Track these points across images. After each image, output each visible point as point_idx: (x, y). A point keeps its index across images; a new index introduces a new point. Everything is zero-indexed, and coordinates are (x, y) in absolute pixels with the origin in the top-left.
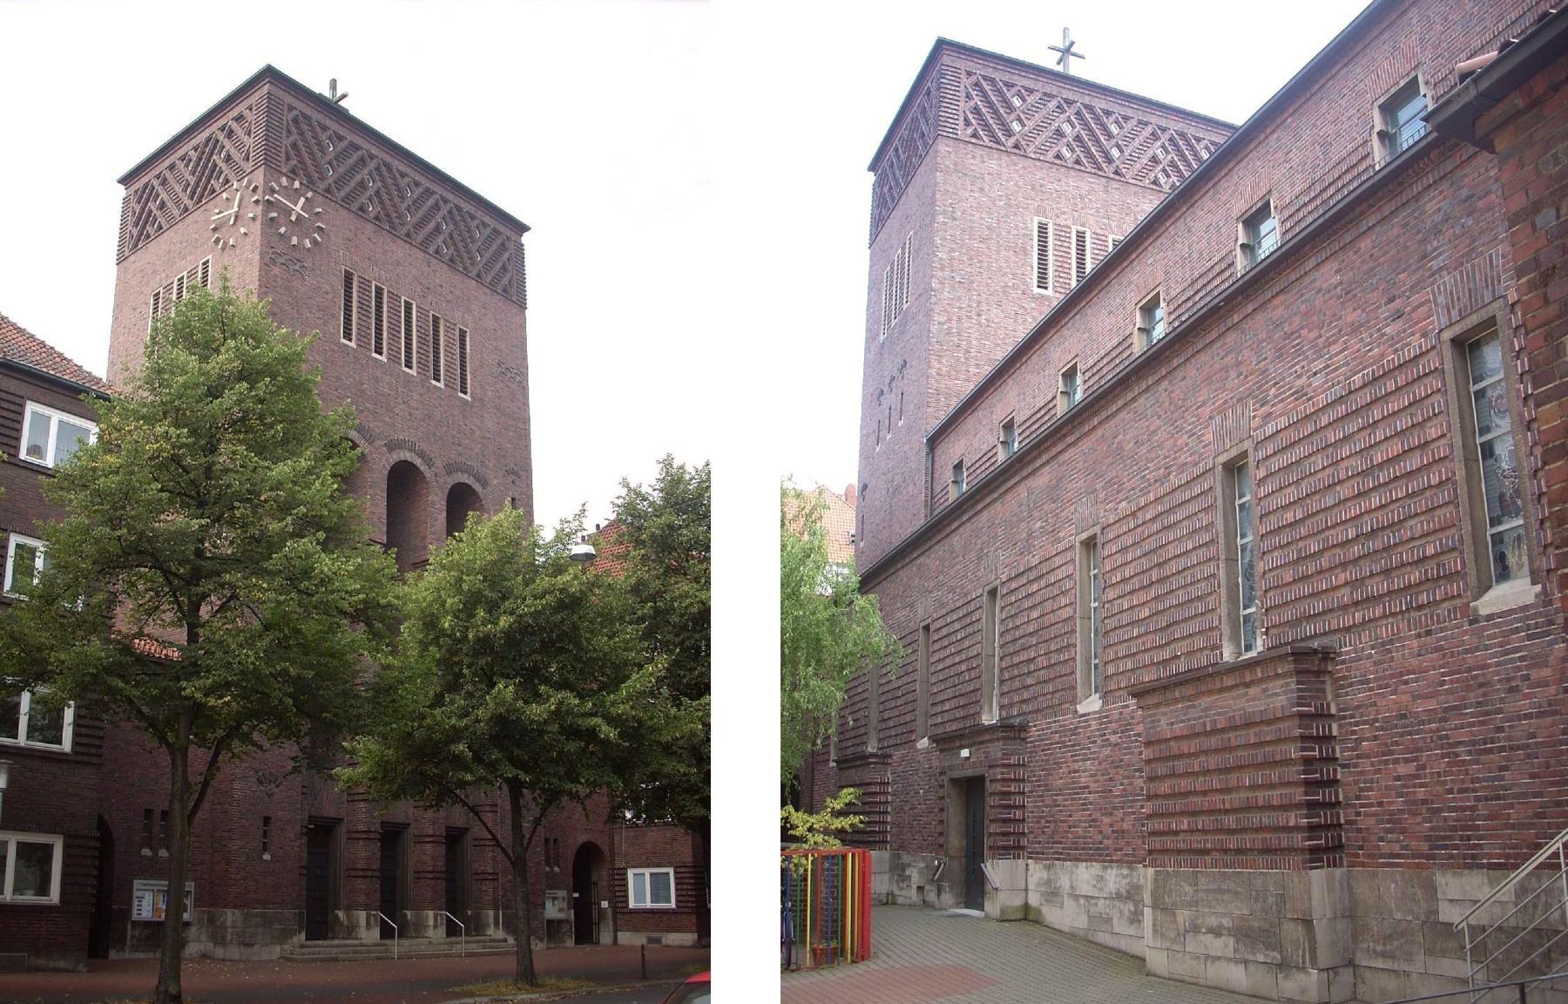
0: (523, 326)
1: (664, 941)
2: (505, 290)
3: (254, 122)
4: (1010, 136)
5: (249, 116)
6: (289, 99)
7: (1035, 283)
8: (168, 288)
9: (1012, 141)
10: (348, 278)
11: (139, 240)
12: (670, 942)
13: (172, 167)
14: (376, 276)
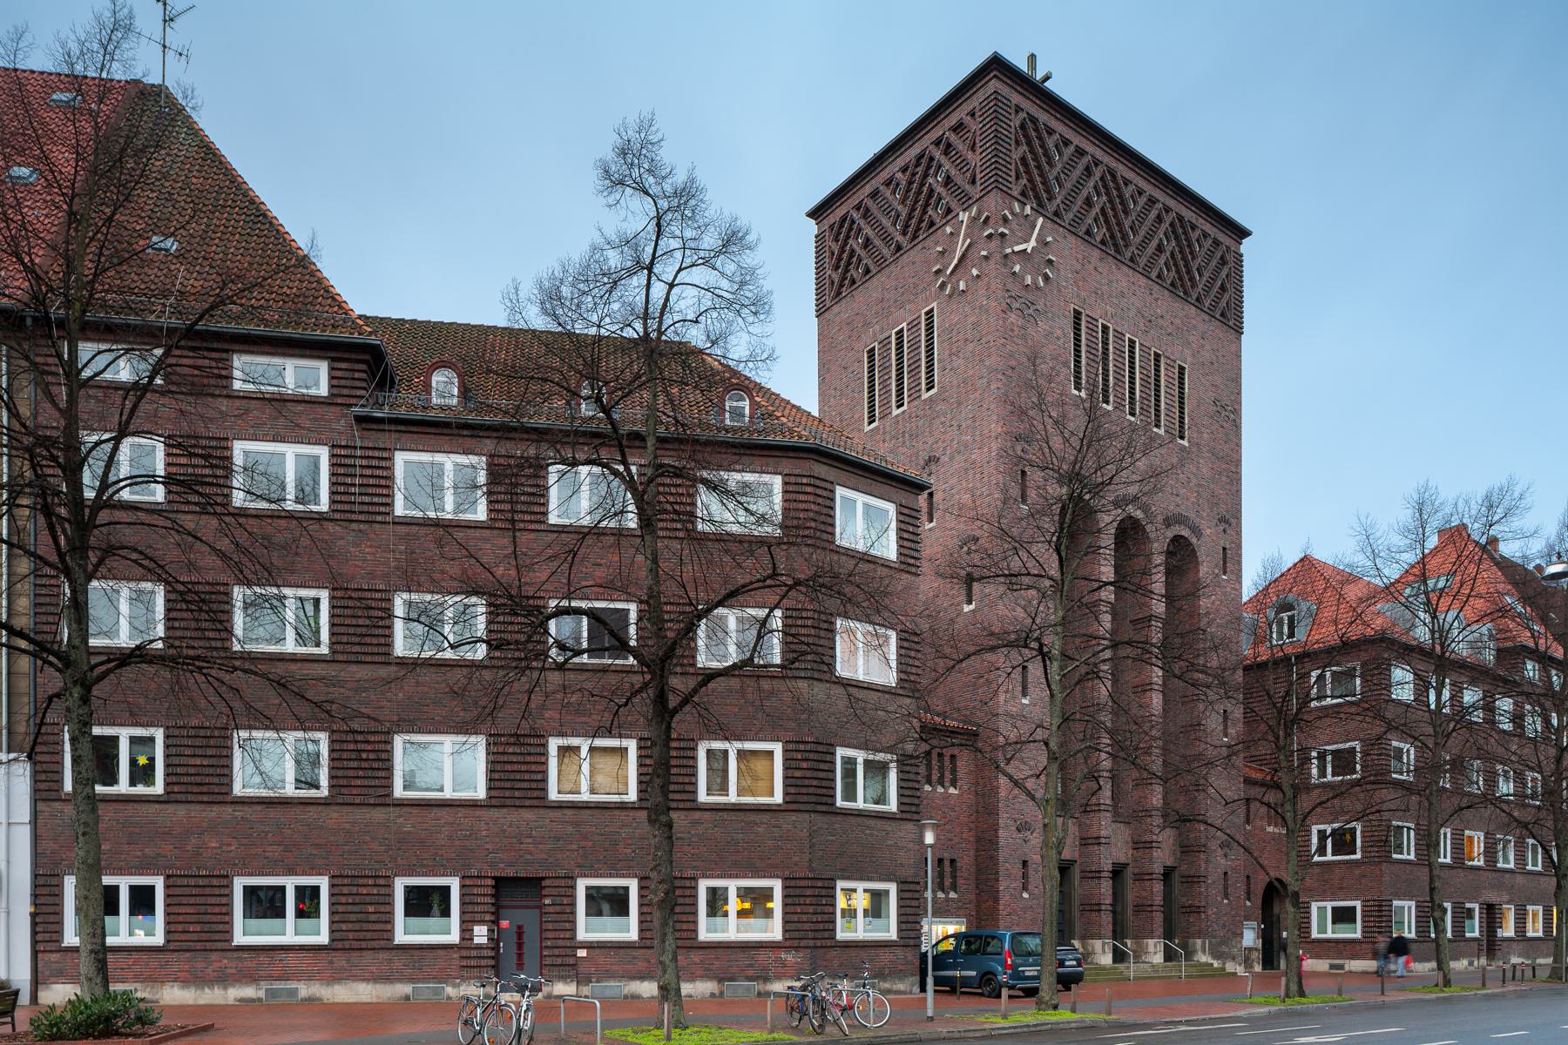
0: (1238, 356)
1: (1347, 968)
2: (1222, 315)
3: (978, 133)
5: (974, 126)
6: (1016, 98)
8: (885, 343)
10: (1077, 314)
11: (841, 286)
12: (1353, 969)
13: (875, 194)
14: (1100, 312)
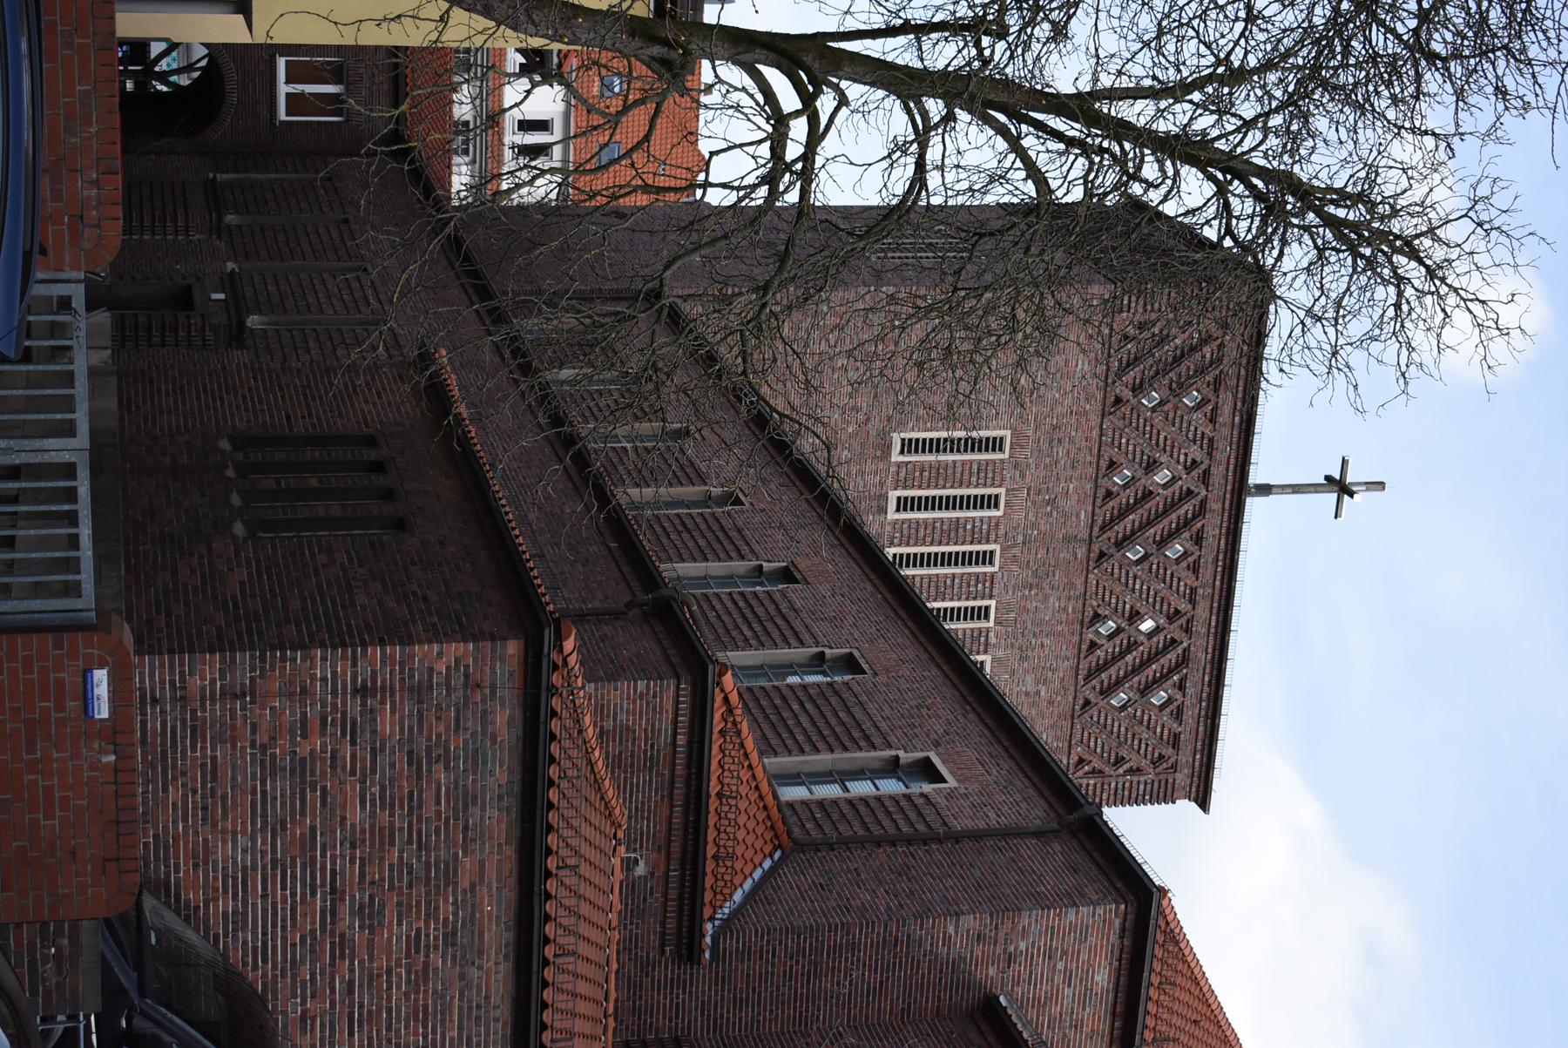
4: (1133, 390)
7: (908, 435)
9: (1127, 394)
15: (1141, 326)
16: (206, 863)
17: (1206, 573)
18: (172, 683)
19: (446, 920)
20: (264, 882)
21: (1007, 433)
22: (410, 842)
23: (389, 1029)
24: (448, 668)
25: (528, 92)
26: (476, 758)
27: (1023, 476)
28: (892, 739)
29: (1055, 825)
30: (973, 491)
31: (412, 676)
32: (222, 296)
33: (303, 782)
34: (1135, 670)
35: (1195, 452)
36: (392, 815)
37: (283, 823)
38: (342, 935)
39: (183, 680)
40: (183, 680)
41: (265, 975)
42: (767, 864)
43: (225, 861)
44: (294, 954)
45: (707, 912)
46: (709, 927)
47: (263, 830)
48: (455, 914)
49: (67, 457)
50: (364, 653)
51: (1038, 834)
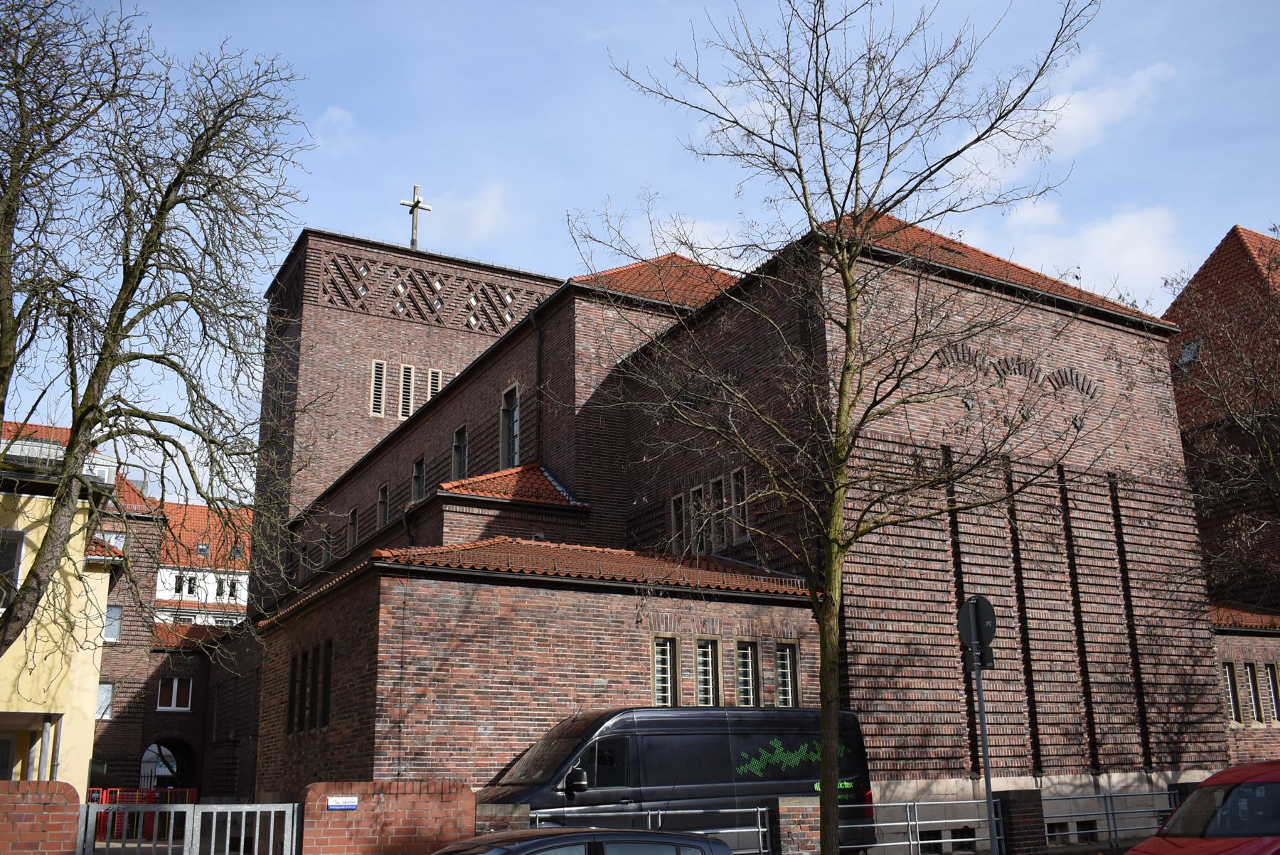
7: (371, 409)
9: (359, 302)
15: (325, 292)
16: (491, 750)
17: (450, 271)
18: (390, 765)
19: (531, 625)
20: (503, 719)
21: (374, 361)
22: (488, 642)
23: (587, 657)
24: (393, 618)
25: (69, 559)
26: (444, 605)
27: (396, 355)
28: (495, 413)
29: (538, 332)
30: (402, 379)
31: (397, 637)
32: (847, 785)
33: (450, 697)
34: (494, 308)
35: (390, 272)
36: (472, 651)
37: (471, 708)
38: (535, 679)
39: (389, 759)
40: (389, 759)
41: (553, 720)
42: (546, 474)
43: (490, 740)
44: (543, 705)
45: (565, 503)
46: (572, 503)
47: (474, 719)
48: (528, 620)
49: (198, 818)
50: (382, 662)
51: (541, 341)
